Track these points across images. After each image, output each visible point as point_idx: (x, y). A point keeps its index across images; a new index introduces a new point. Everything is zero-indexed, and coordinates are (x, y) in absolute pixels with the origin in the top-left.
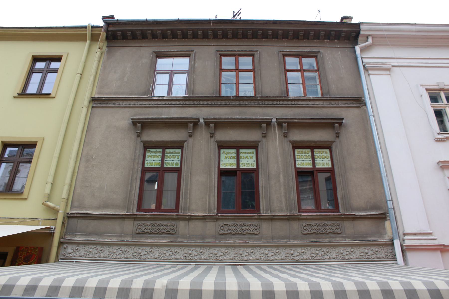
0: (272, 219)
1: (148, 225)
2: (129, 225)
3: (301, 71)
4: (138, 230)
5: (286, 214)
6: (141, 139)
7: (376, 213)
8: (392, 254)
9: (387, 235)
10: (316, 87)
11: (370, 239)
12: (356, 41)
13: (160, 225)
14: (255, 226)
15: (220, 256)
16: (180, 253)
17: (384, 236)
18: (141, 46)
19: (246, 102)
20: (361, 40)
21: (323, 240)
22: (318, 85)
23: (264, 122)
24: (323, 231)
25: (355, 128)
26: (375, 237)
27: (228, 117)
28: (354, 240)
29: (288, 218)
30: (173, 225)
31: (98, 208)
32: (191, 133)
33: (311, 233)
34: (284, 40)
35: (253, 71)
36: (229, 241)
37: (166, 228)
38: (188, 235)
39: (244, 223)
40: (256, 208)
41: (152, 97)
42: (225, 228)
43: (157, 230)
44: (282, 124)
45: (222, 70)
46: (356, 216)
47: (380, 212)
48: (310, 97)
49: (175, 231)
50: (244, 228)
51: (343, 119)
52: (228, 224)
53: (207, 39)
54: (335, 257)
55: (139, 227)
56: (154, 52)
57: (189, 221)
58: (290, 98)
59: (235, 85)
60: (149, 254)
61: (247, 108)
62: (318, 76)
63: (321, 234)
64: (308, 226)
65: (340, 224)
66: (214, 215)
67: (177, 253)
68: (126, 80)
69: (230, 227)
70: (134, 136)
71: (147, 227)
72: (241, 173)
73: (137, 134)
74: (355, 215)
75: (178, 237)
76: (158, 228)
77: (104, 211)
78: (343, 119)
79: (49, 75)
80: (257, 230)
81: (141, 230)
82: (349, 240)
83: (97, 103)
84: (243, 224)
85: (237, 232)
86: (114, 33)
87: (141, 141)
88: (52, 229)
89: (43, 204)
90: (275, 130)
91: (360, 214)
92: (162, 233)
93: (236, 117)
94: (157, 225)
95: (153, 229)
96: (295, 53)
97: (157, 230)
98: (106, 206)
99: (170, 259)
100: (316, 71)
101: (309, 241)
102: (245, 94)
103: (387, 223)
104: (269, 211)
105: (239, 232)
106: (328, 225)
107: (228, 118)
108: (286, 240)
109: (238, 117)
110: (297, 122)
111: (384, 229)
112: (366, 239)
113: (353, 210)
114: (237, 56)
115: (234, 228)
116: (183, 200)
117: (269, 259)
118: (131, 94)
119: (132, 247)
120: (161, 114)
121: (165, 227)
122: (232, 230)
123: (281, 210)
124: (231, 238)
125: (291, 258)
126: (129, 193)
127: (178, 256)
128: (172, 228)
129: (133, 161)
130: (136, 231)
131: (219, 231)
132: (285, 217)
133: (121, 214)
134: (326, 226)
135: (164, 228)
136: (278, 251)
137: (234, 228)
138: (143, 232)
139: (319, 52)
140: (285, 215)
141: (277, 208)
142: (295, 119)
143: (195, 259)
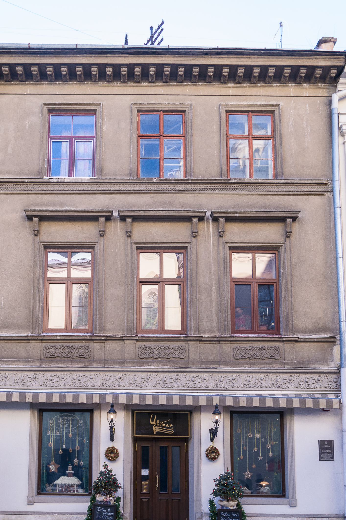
3: (249, 137)
4: (47, 354)
5: (217, 335)
7: (324, 336)
8: (336, 383)
9: (334, 362)
11: (312, 366)
12: (335, 84)
13: (262, 349)
19: (172, 187)
20: (343, 83)
21: (258, 366)
23: (36, 216)
24: (164, 355)
26: (319, 364)
27: (150, 210)
28: (294, 367)
30: (182, 348)
33: (245, 358)
35: (182, 138)
36: (151, 366)
37: (79, 351)
38: (104, 359)
40: (277, 330)
41: (49, 178)
43: (69, 354)
44: (219, 219)
45: (273, 137)
47: (329, 335)
48: (259, 180)
50: (169, 351)
51: (298, 213)
54: (242, 385)
56: (45, 104)
62: (272, 145)
64: (242, 349)
65: (279, 348)
66: (133, 335)
67: (93, 379)
68: (10, 151)
72: (257, 285)
74: (299, 338)
75: (93, 362)
78: (298, 213)
80: (88, 353)
81: (146, 354)
85: (161, 356)
91: (305, 337)
92: (74, 357)
93: (160, 209)
94: (68, 348)
95: (64, 353)
96: (242, 108)
97: (69, 354)
100: (270, 137)
102: (171, 175)
103: (336, 349)
104: (198, 332)
105: (162, 356)
107: (150, 211)
109: (162, 209)
111: (332, 355)
112: (308, 367)
115: (156, 351)
116: (97, 319)
117: (195, 386)
118: (20, 174)
120: (62, 205)
122: (154, 353)
123: (211, 331)
124: (154, 363)
125: (134, 385)
126: (32, 310)
128: (86, 351)
129: (33, 269)
130: (44, 354)
131: (139, 354)
134: (168, 349)
135: (172, 352)
137: (61, 351)
138: (52, 356)
139: (278, 105)
140: (216, 336)
141: (207, 329)
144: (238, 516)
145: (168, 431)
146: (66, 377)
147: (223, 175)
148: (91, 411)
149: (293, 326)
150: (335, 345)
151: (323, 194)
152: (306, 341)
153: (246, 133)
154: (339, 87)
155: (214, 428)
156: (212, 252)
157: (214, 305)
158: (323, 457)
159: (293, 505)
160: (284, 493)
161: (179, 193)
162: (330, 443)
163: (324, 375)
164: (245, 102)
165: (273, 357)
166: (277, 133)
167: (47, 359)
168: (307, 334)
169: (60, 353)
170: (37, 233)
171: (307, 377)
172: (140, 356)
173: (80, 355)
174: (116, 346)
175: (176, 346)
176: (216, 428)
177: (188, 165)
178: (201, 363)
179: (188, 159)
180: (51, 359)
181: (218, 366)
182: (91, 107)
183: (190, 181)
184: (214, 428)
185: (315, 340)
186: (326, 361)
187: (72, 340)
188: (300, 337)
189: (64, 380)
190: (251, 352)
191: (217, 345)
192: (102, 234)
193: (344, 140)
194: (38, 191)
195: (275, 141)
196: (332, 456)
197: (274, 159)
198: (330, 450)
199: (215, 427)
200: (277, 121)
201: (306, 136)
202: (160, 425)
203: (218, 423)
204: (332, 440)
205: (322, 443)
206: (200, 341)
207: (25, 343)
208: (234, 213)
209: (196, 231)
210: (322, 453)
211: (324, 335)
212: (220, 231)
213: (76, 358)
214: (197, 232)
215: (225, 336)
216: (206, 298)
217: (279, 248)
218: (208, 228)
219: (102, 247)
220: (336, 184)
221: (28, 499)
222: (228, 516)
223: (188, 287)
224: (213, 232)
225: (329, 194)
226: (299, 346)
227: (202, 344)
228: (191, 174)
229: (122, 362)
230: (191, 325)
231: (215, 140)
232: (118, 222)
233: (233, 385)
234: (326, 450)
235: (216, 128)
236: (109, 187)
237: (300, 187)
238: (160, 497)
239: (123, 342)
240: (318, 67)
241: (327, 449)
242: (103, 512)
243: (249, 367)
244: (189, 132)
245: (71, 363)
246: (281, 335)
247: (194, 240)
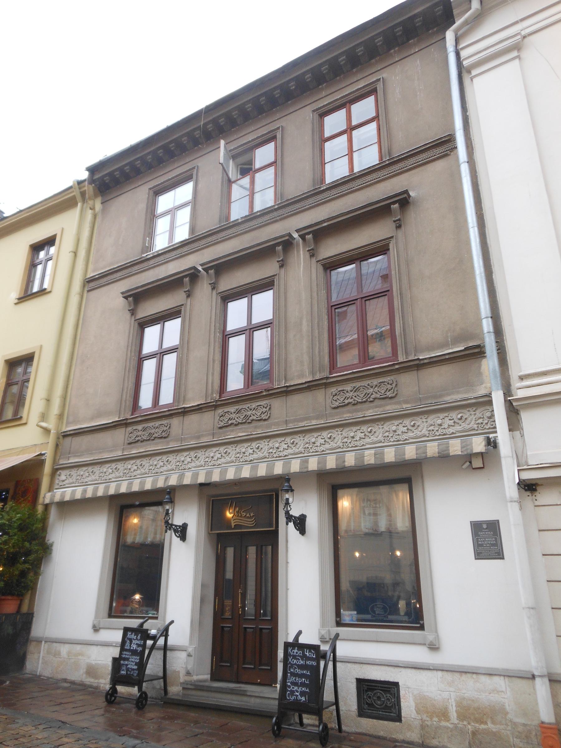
1: (233, 413)
2: (120, 435)
6: (135, 318)
14: (388, 383)
15: (217, 460)
16: (231, 453)
17: (478, 387)
23: (278, 244)
25: (435, 199)
26: (458, 393)
29: (308, 386)
31: (92, 419)
32: (399, 220)
34: (320, 87)
37: (378, 389)
39: (370, 383)
46: (422, 362)
49: (395, 393)
52: (345, 389)
53: (212, 140)
55: (335, 398)
57: (184, 416)
58: (322, 189)
60: (458, 423)
61: (262, 229)
63: (242, 423)
69: (232, 415)
70: (128, 315)
71: (348, 395)
73: (394, 223)
76: (365, 392)
77: (97, 422)
78: (406, 192)
79: (355, 133)
83: (92, 285)
85: (359, 400)
87: (318, 262)
89: (38, 425)
90: (298, 251)
94: (363, 388)
98: (99, 415)
99: (362, 444)
101: (341, 418)
106: (372, 387)
108: (306, 422)
110: (328, 225)
112: (441, 400)
113: (422, 351)
114: (348, 105)
117: (280, 455)
119: (470, 409)
121: (376, 388)
125: (438, 433)
127: (143, 471)
132: (304, 386)
133: (111, 421)
136: (461, 415)
141: (296, 374)
142: (324, 221)
143: (451, 433)
144: (315, 657)
145: (249, 523)
146: (334, 436)
148: (408, 481)
157: (304, 342)
158: (481, 553)
159: (434, 647)
168: (435, 352)
169: (352, 398)
171: (440, 416)
173: (381, 396)
188: (421, 358)
189: (259, 450)
196: (499, 549)
198: (494, 539)
201: (418, 97)
202: (240, 515)
204: (471, 524)
205: (477, 527)
208: (322, 224)
213: (376, 400)
216: (295, 336)
221: (319, 632)
222: (300, 656)
234: (487, 539)
238: (261, 625)
242: (133, 639)
243: (351, 415)
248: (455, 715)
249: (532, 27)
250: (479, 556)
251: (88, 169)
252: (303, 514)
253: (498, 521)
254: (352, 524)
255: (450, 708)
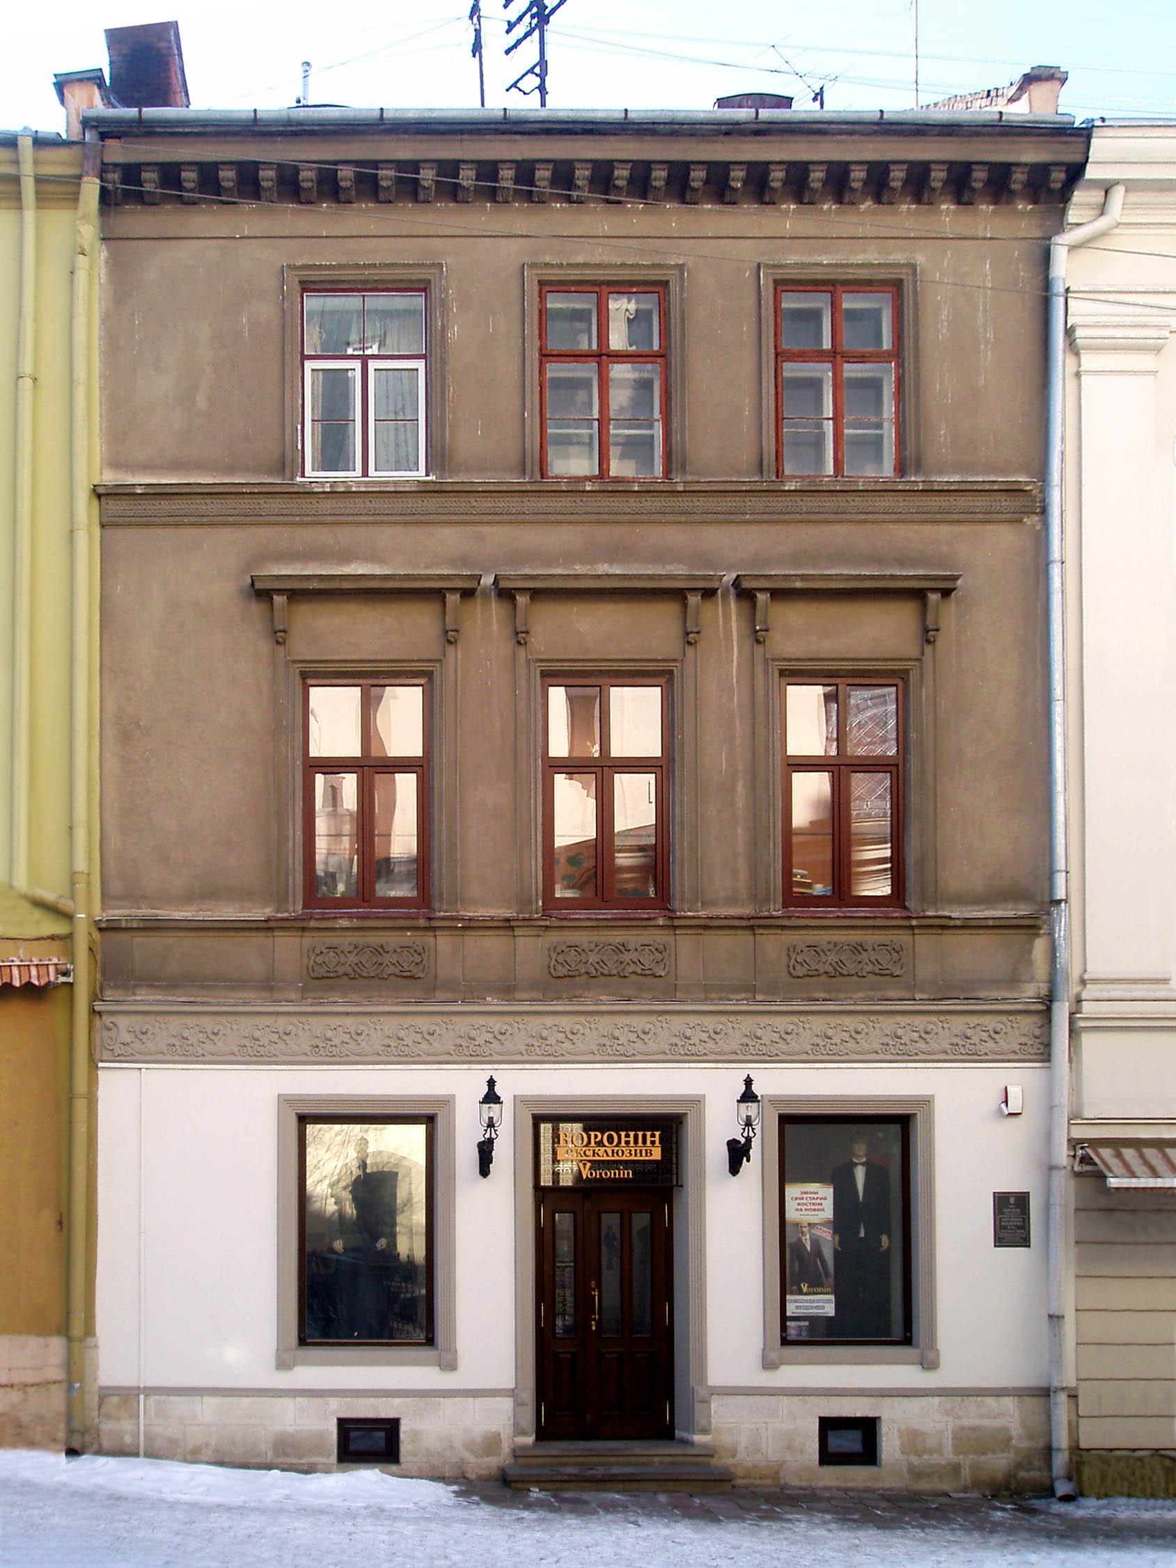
0: (706, 926)
10: (651, 427)
12: (1062, 205)
13: (859, 948)
18: (235, 238)
19: (633, 503)
21: (849, 995)
22: (656, 424)
23: (279, 591)
31: (189, 898)
42: (330, 961)
47: (1024, 910)
50: (626, 957)
51: (955, 578)
59: (831, 422)
68: (201, 402)
74: (950, 918)
78: (955, 578)
82: (925, 996)
83: (115, 506)
84: (382, 947)
86: (131, 173)
88: (72, 963)
103: (1040, 945)
117: (693, 1052)
123: (732, 900)
128: (418, 959)
141: (722, 894)
147: (765, 468)
149: (936, 885)
150: (1038, 935)
151: (1021, 521)
152: (968, 926)
153: (827, 344)
154: (1073, 216)
155: (743, 1141)
156: (738, 686)
158: (1003, 1238)
159: (929, 1364)
160: (908, 1334)
161: (652, 519)
162: (1022, 1200)
163: (1010, 1018)
164: (826, 259)
165: (888, 972)
166: (909, 343)
167: (317, 982)
170: (279, 637)
172: (552, 971)
174: (493, 944)
175: (645, 943)
176: (749, 1140)
177: (676, 438)
178: (707, 989)
179: (675, 423)
180: (325, 982)
181: (749, 995)
182: (416, 274)
183: (680, 488)
184: (743, 1141)
185: (991, 923)
186: (1014, 981)
187: (377, 928)
188: (953, 915)
190: (833, 958)
191: (745, 938)
192: (450, 638)
193: (1080, 366)
194: (281, 518)
195: (900, 365)
197: (897, 418)
199: (746, 1138)
200: (908, 312)
203: (751, 1125)
205: (1001, 1201)
206: (706, 927)
207: (260, 939)
209: (695, 630)
210: (1002, 1228)
211: (1012, 910)
212: (758, 628)
214: (698, 633)
215: (766, 914)
217: (907, 671)
218: (727, 618)
219: (451, 672)
220: (1055, 497)
223: (674, 781)
224: (739, 631)
225: (1036, 518)
226: (949, 939)
227: (708, 937)
228: (683, 466)
229: (507, 990)
230: (682, 886)
231: (746, 368)
232: (493, 599)
233: (786, 1047)
235: (747, 330)
236: (468, 505)
237: (962, 502)
239: (511, 933)
240: (1017, 164)
241: (1013, 1219)
244: (678, 342)
245: (377, 993)
246: (905, 908)
247: (690, 651)
248: (950, 1448)
249: (1130, 295)
250: (1000, 1242)
251: (116, 37)
252: (734, 1140)
253: (174, 26)
254: (770, 1451)
255: (945, 1441)
